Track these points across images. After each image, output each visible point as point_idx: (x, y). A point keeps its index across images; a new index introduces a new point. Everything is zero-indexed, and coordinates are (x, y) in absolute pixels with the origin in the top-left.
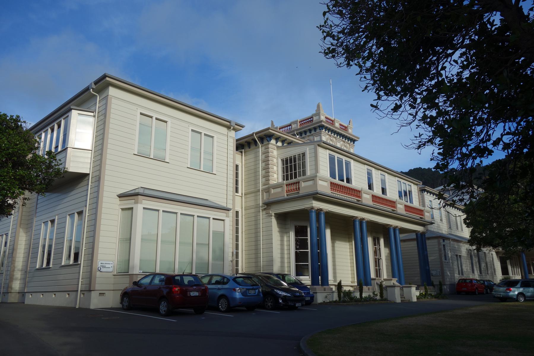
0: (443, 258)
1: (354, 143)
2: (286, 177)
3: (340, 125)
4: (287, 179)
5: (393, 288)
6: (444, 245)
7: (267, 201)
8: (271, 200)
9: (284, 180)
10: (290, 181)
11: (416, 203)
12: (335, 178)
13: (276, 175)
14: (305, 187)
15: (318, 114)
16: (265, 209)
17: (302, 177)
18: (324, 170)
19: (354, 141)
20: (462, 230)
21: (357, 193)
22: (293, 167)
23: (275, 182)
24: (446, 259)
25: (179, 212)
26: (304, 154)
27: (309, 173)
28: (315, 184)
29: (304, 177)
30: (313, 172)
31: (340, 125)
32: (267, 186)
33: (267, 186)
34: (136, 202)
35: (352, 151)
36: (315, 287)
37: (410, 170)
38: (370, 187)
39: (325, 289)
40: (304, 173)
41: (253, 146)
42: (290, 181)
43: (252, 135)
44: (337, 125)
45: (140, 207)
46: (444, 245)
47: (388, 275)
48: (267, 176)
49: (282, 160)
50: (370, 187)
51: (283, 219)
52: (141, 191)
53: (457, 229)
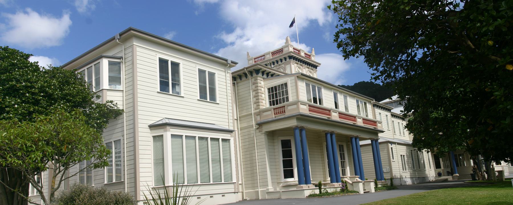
0: (391, 158)
1: (316, 68)
2: (272, 103)
3: (305, 54)
4: (274, 105)
5: (302, 191)
6: (392, 148)
7: (259, 122)
8: (262, 121)
9: (271, 105)
10: (276, 106)
11: (370, 117)
12: (317, 103)
13: (265, 103)
14: (290, 111)
15: (287, 46)
16: (258, 128)
17: (286, 103)
18: (303, 96)
19: (315, 67)
20: (404, 134)
21: (328, 111)
22: (277, 95)
23: (264, 107)
24: (393, 159)
25: (184, 135)
26: (286, 84)
27: (291, 99)
28: (298, 108)
29: (288, 102)
30: (295, 97)
31: (305, 54)
32: (258, 110)
33: (258, 110)
34: (166, 131)
35: (315, 76)
36: (302, 185)
37: (356, 84)
38: (336, 107)
39: (309, 187)
40: (288, 100)
41: (244, 78)
42: (276, 106)
43: (243, 69)
44: (303, 54)
45: (168, 134)
46: (392, 148)
47: (351, 174)
48: (257, 103)
49: (269, 89)
50: (336, 107)
51: (272, 135)
52: (167, 121)
53: (400, 133)
